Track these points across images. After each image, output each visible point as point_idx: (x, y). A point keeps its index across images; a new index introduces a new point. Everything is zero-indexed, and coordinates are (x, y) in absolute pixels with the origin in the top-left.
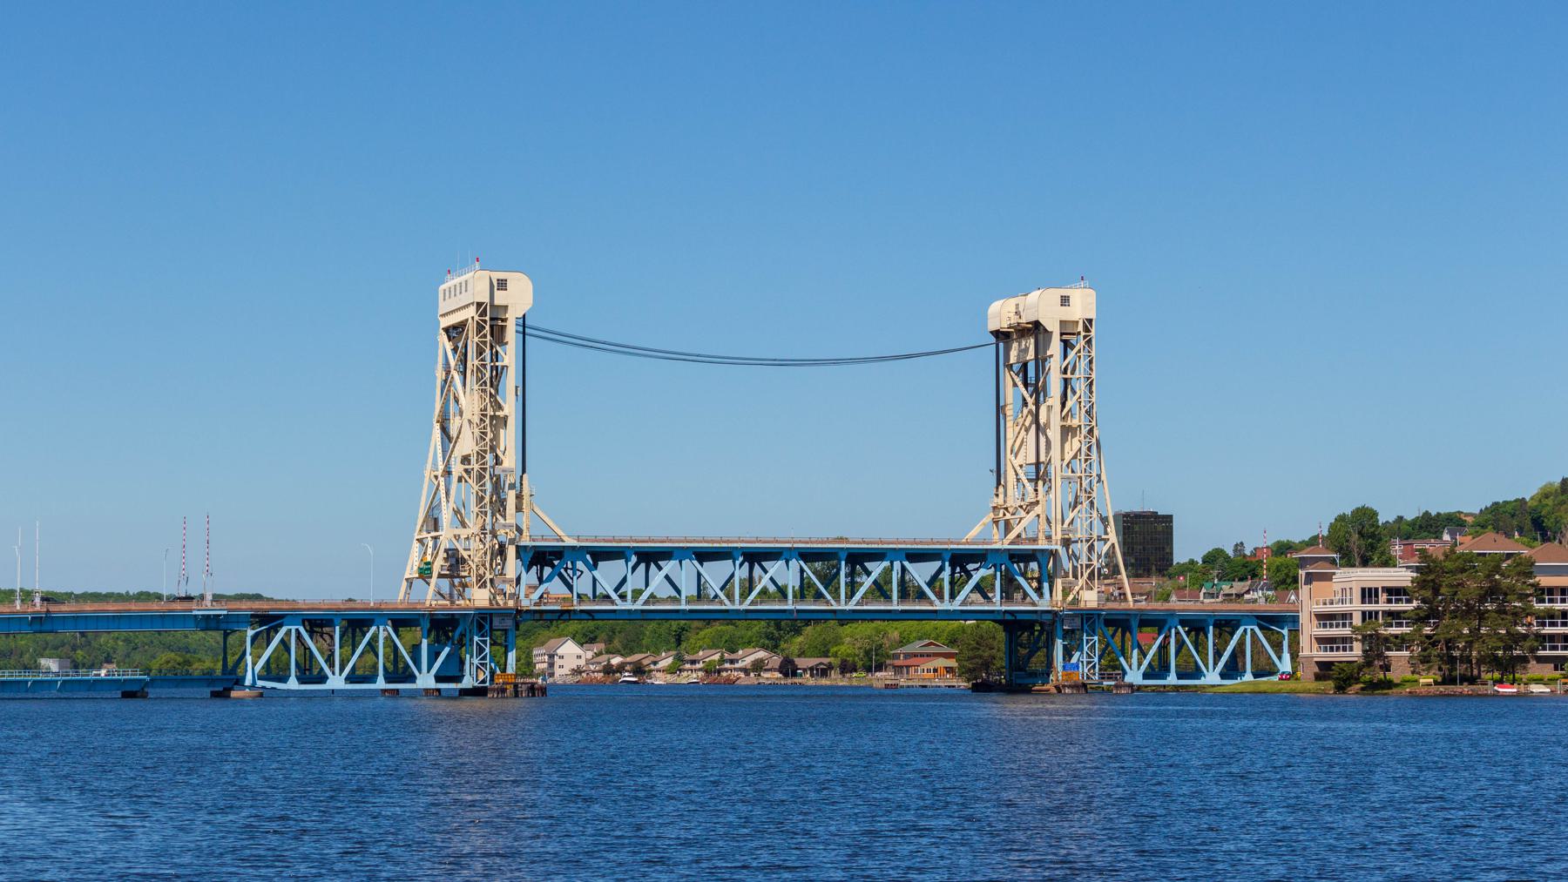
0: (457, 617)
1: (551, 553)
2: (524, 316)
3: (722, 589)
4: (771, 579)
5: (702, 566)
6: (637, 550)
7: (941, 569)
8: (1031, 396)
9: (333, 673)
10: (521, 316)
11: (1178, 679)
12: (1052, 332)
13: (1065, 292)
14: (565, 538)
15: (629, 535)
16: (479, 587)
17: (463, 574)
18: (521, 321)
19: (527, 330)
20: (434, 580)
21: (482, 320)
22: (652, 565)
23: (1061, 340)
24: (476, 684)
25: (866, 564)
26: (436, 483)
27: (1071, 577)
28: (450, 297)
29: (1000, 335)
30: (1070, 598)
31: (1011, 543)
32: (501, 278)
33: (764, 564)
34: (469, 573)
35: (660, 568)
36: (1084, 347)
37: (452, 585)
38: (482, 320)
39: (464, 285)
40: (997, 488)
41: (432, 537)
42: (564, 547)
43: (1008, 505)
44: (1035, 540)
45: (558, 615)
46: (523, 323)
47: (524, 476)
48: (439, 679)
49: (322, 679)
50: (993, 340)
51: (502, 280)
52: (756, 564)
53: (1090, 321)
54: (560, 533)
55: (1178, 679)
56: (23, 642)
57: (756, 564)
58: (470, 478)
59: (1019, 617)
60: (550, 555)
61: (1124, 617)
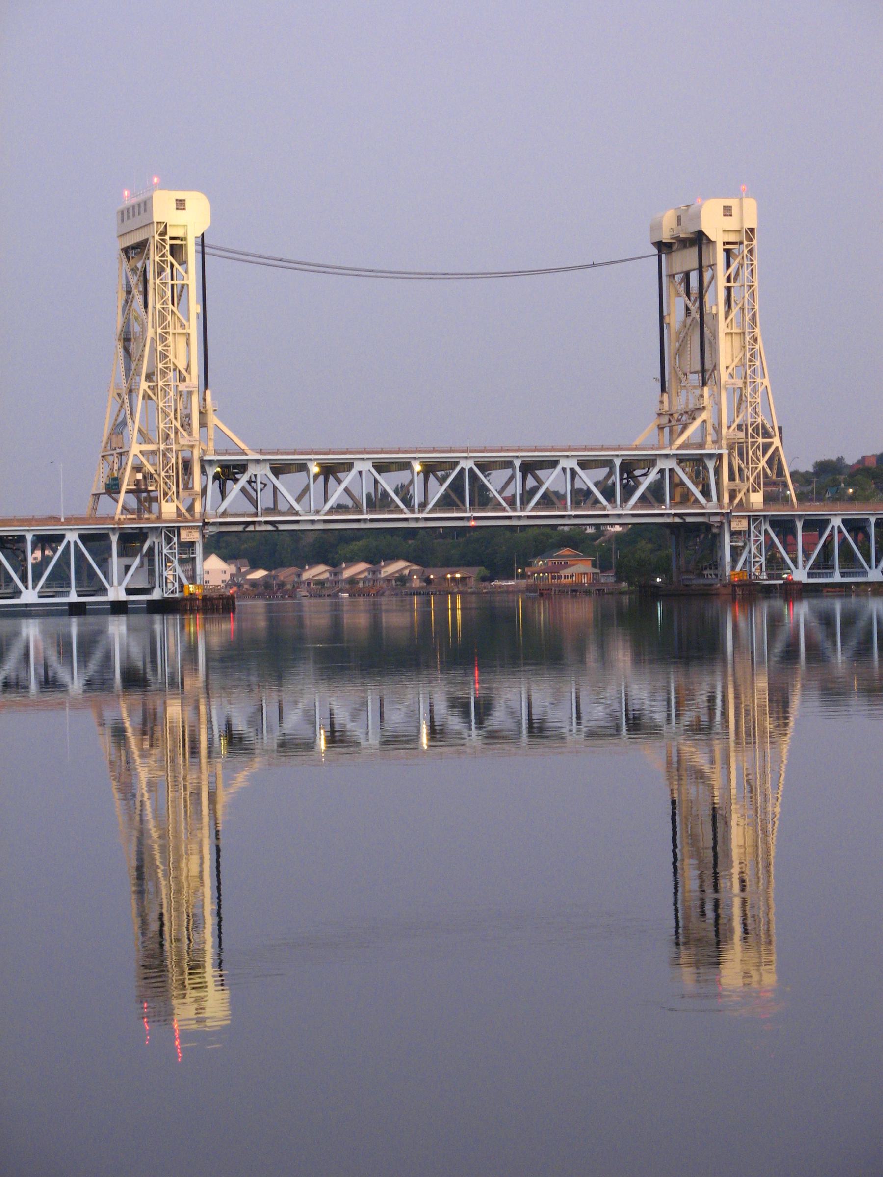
0: (145, 531)
1: (235, 467)
2: (203, 235)
3: (298, 500)
4: (346, 490)
5: (277, 477)
6: (224, 463)
7: (512, 477)
8: (694, 304)
9: (27, 588)
10: (199, 235)
11: (842, 576)
12: (715, 242)
13: (180, 195)
14: (248, 452)
15: (432, 446)
16: (167, 501)
17: (150, 488)
18: (200, 240)
19: (206, 249)
20: (122, 496)
21: (161, 240)
22: (331, 477)
23: (725, 250)
24: (166, 596)
25: (536, 472)
26: (120, 401)
27: (737, 481)
28: (134, 215)
29: (663, 247)
30: (737, 501)
31: (678, 449)
32: (726, 205)
33: (339, 475)
34: (157, 487)
35: (339, 482)
36: (746, 255)
37: (139, 500)
38: (161, 240)
39: (142, 205)
40: (662, 396)
41: (117, 453)
42: (247, 460)
43: (674, 410)
44: (701, 446)
45: (244, 526)
46: (202, 241)
47: (207, 392)
48: (129, 592)
49: (17, 593)
50: (656, 251)
51: (180, 200)
52: (529, 475)
53: (752, 230)
54: (243, 446)
55: (842, 576)
56: (504, 548)
57: (331, 476)
58: (154, 394)
59: (689, 520)
60: (234, 468)
61: (789, 518)
